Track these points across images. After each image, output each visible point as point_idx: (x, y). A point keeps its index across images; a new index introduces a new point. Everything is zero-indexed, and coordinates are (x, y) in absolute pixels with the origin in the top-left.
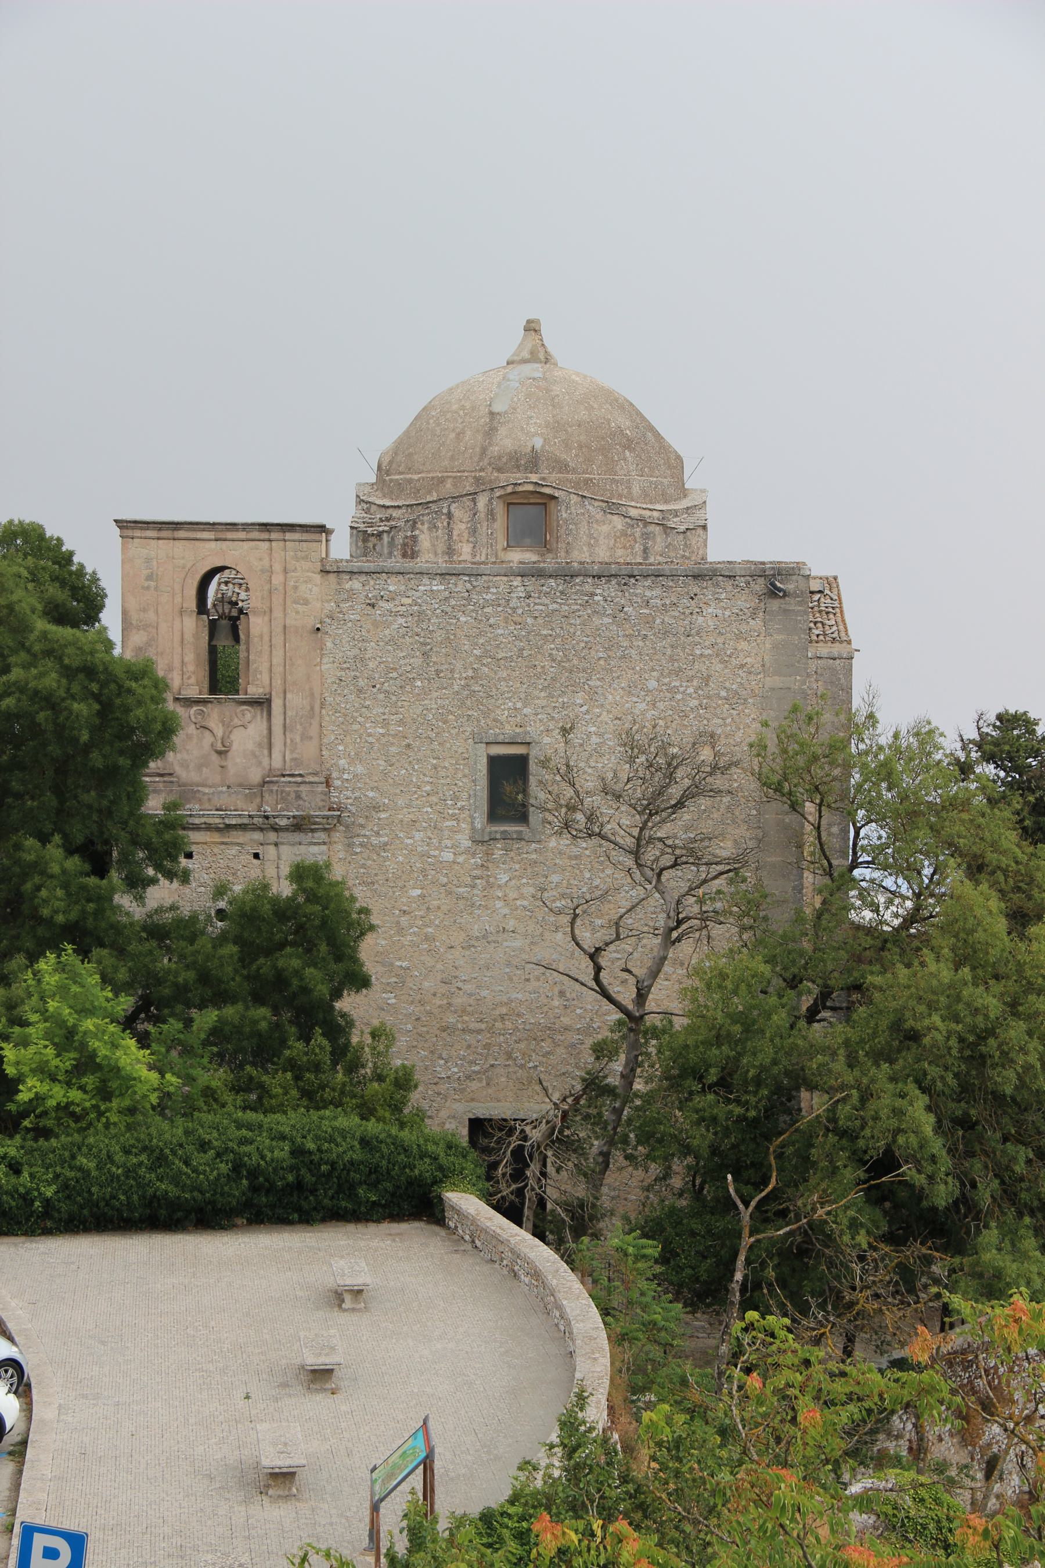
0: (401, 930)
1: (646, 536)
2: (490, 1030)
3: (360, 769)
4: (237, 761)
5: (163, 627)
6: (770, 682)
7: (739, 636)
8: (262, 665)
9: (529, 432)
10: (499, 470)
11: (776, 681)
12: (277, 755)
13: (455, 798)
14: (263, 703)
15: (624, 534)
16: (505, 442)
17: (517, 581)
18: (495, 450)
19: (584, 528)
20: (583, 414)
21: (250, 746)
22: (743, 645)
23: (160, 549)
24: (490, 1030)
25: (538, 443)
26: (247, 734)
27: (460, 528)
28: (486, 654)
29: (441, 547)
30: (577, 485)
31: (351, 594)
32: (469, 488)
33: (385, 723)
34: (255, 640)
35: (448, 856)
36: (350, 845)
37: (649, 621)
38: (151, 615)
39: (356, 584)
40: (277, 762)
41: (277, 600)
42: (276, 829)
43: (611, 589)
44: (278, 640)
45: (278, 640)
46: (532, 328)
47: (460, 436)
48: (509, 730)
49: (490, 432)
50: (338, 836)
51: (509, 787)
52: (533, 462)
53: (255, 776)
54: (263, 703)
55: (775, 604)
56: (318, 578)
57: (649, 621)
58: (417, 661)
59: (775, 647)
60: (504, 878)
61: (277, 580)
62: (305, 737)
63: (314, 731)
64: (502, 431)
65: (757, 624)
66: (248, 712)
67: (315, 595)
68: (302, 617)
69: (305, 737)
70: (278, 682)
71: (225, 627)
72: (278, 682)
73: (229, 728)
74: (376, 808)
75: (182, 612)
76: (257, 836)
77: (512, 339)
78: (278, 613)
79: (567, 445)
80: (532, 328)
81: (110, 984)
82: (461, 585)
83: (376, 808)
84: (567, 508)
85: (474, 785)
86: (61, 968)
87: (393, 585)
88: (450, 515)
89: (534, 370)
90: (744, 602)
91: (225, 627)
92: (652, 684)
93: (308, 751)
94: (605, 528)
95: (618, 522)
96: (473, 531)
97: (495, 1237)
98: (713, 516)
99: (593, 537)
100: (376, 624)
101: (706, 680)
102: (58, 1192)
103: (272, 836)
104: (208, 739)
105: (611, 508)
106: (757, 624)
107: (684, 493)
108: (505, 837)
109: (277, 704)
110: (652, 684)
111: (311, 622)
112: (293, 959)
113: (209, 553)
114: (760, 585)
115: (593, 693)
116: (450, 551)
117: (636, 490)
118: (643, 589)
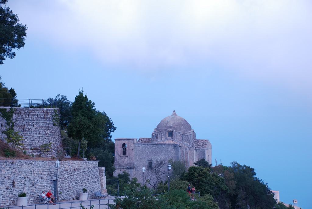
1: (182, 136)
3: (136, 163)
4: (125, 162)
5: (118, 149)
7: (172, 151)
8: (128, 153)
9: (171, 124)
10: (167, 128)
11: (175, 155)
14: (127, 156)
16: (168, 125)
18: (167, 126)
20: (177, 122)
21: (126, 160)
25: (172, 125)
26: (126, 159)
36: (135, 170)
38: (117, 148)
40: (129, 162)
41: (129, 146)
43: (160, 146)
44: (129, 150)
45: (129, 150)
46: (174, 111)
47: (164, 124)
49: (167, 124)
50: (134, 169)
52: (171, 127)
55: (175, 148)
56: (133, 144)
58: (142, 152)
61: (129, 144)
62: (131, 160)
64: (168, 124)
65: (174, 150)
67: (133, 146)
68: (131, 148)
73: (124, 158)
75: (120, 148)
77: (172, 113)
78: (129, 148)
80: (174, 111)
82: (146, 145)
83: (138, 167)
85: (146, 163)
86: (205, 196)
90: (173, 147)
93: (132, 161)
94: (178, 135)
96: (164, 135)
101: (169, 155)
103: (128, 169)
106: (174, 150)
109: (129, 157)
111: (132, 149)
113: (123, 142)
114: (174, 146)
117: (183, 130)
118: (163, 146)
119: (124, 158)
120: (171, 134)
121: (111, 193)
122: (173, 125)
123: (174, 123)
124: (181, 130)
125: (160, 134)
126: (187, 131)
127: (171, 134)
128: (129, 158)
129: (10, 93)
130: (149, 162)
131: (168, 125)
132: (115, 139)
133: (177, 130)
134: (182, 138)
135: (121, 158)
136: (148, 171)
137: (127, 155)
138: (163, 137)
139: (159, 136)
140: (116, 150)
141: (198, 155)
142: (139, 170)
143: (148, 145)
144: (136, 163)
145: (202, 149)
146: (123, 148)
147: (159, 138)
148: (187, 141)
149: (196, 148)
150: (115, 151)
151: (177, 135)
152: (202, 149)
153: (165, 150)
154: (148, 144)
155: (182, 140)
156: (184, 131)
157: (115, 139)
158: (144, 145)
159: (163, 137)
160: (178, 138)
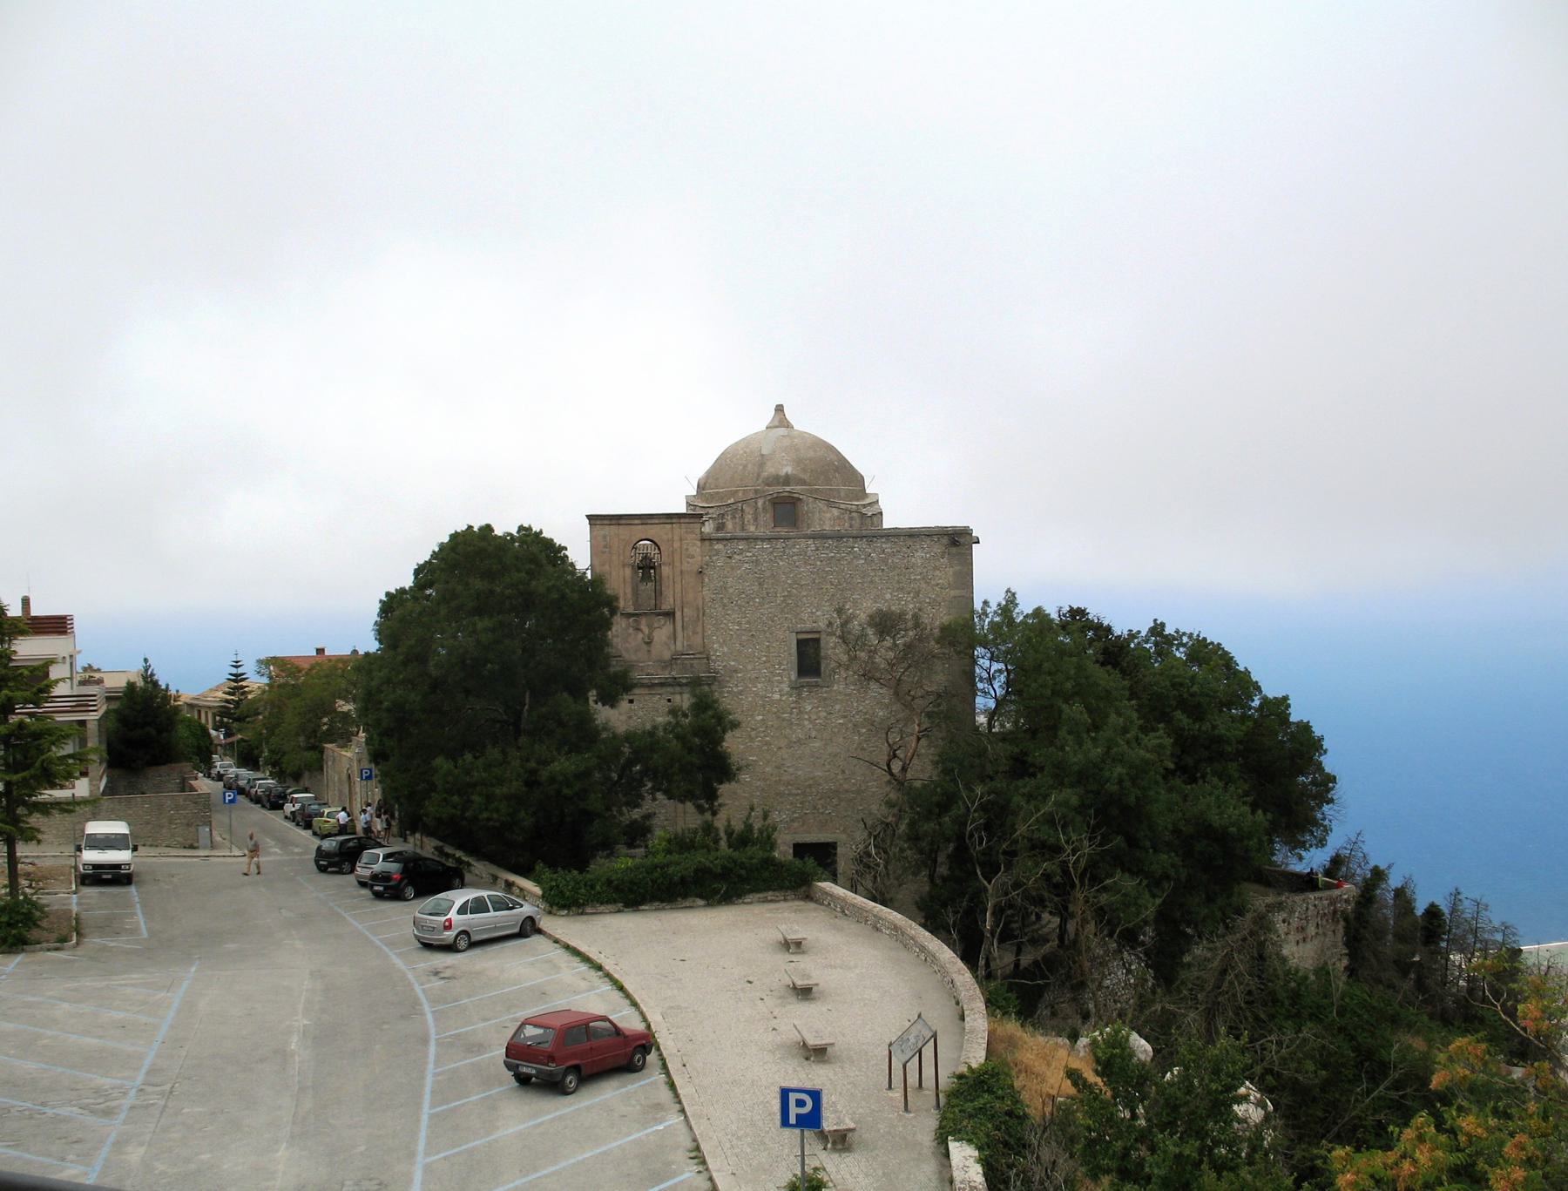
0: (752, 739)
1: (851, 519)
2: (804, 793)
6: (953, 593)
12: (679, 644)
13: (780, 664)
14: (670, 615)
16: (770, 470)
18: (765, 474)
23: (613, 530)
24: (804, 793)
27: (748, 517)
28: (795, 582)
30: (811, 491)
31: (718, 552)
32: (752, 495)
33: (739, 624)
34: (665, 579)
35: (777, 697)
39: (719, 546)
41: (677, 558)
42: (680, 685)
43: (863, 544)
44: (678, 579)
45: (678, 579)
46: (146, 660)
48: (809, 626)
49: (762, 465)
51: (809, 658)
52: (787, 480)
53: (667, 655)
54: (670, 615)
55: (954, 550)
57: (884, 561)
58: (756, 588)
59: (955, 573)
60: (809, 708)
61: (676, 545)
62: (695, 633)
63: (699, 629)
64: (769, 464)
67: (696, 549)
68: (693, 565)
69: (695, 633)
70: (678, 602)
71: (647, 568)
72: (678, 602)
74: (736, 671)
76: (670, 689)
78: (677, 564)
79: (804, 470)
80: (146, 660)
82: (780, 544)
83: (736, 671)
84: (809, 506)
85: (788, 656)
89: (782, 431)
90: (937, 549)
91: (647, 568)
92: (888, 596)
93: (697, 640)
95: (836, 512)
96: (756, 519)
97: (861, 909)
98: (884, 505)
99: (824, 518)
101: (918, 593)
102: (1410, 1026)
104: (640, 636)
105: (830, 504)
107: (865, 495)
108: (809, 685)
109: (678, 614)
110: (888, 596)
111: (696, 568)
112: (698, 755)
114: (945, 541)
116: (743, 529)
119: (650, 626)
130: (799, 642)
131: (772, 470)
132: (589, 517)
135: (629, 626)
136: (799, 695)
142: (740, 693)
143: (790, 543)
153: (894, 568)
157: (589, 517)
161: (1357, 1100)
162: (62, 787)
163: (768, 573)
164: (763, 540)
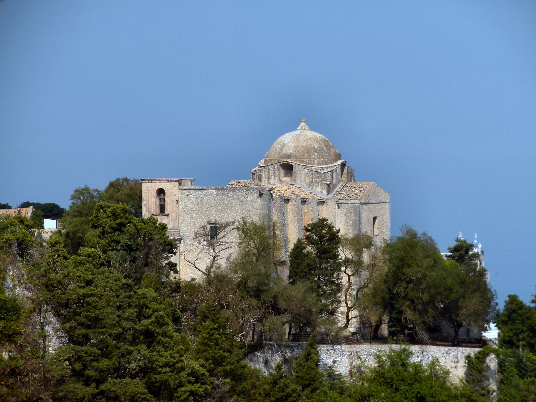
1: (312, 174)
3: (186, 229)
7: (255, 202)
10: (282, 158)
11: (262, 211)
14: (168, 215)
15: (307, 173)
16: (284, 151)
17: (214, 191)
19: (299, 172)
20: (305, 144)
22: (256, 204)
25: (291, 151)
27: (271, 172)
28: (209, 206)
29: (267, 177)
33: (191, 219)
37: (238, 199)
39: (185, 191)
52: (289, 156)
54: (168, 215)
57: (238, 199)
58: (196, 207)
62: (175, 222)
64: (284, 148)
66: (165, 217)
81: (382, 318)
82: (204, 191)
83: (189, 236)
87: (192, 192)
88: (269, 169)
92: (239, 212)
93: (176, 225)
94: (303, 172)
96: (274, 173)
100: (189, 200)
101: (249, 211)
109: (170, 216)
110: (239, 212)
115: (228, 214)
117: (316, 162)
118: (237, 193)
120: (288, 168)
121: (107, 380)
122: (293, 151)
123: (297, 147)
124: (312, 162)
125: (265, 172)
126: (326, 165)
127: (288, 168)
128: (171, 219)
129: (299, 247)
133: (302, 161)
134: (311, 180)
137: (166, 213)
138: (272, 177)
139: (263, 175)
140: (144, 203)
141: (345, 215)
144: (186, 229)
145: (353, 202)
146: (160, 199)
147: (263, 179)
148: (321, 186)
149: (340, 201)
150: (143, 206)
151: (300, 172)
152: (353, 202)
154: (209, 188)
155: (312, 182)
156: (319, 163)
158: (200, 192)
159: (272, 177)
160: (303, 178)
161: (306, 380)
162: (286, 330)
163: (200, 202)
164: (199, 190)
